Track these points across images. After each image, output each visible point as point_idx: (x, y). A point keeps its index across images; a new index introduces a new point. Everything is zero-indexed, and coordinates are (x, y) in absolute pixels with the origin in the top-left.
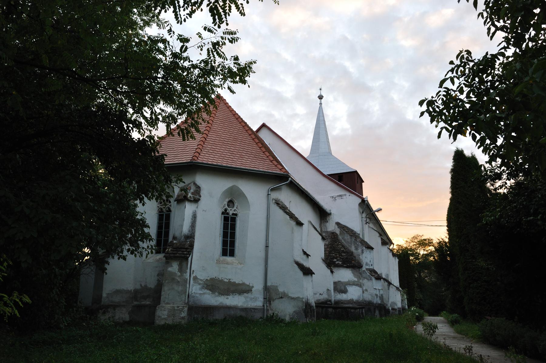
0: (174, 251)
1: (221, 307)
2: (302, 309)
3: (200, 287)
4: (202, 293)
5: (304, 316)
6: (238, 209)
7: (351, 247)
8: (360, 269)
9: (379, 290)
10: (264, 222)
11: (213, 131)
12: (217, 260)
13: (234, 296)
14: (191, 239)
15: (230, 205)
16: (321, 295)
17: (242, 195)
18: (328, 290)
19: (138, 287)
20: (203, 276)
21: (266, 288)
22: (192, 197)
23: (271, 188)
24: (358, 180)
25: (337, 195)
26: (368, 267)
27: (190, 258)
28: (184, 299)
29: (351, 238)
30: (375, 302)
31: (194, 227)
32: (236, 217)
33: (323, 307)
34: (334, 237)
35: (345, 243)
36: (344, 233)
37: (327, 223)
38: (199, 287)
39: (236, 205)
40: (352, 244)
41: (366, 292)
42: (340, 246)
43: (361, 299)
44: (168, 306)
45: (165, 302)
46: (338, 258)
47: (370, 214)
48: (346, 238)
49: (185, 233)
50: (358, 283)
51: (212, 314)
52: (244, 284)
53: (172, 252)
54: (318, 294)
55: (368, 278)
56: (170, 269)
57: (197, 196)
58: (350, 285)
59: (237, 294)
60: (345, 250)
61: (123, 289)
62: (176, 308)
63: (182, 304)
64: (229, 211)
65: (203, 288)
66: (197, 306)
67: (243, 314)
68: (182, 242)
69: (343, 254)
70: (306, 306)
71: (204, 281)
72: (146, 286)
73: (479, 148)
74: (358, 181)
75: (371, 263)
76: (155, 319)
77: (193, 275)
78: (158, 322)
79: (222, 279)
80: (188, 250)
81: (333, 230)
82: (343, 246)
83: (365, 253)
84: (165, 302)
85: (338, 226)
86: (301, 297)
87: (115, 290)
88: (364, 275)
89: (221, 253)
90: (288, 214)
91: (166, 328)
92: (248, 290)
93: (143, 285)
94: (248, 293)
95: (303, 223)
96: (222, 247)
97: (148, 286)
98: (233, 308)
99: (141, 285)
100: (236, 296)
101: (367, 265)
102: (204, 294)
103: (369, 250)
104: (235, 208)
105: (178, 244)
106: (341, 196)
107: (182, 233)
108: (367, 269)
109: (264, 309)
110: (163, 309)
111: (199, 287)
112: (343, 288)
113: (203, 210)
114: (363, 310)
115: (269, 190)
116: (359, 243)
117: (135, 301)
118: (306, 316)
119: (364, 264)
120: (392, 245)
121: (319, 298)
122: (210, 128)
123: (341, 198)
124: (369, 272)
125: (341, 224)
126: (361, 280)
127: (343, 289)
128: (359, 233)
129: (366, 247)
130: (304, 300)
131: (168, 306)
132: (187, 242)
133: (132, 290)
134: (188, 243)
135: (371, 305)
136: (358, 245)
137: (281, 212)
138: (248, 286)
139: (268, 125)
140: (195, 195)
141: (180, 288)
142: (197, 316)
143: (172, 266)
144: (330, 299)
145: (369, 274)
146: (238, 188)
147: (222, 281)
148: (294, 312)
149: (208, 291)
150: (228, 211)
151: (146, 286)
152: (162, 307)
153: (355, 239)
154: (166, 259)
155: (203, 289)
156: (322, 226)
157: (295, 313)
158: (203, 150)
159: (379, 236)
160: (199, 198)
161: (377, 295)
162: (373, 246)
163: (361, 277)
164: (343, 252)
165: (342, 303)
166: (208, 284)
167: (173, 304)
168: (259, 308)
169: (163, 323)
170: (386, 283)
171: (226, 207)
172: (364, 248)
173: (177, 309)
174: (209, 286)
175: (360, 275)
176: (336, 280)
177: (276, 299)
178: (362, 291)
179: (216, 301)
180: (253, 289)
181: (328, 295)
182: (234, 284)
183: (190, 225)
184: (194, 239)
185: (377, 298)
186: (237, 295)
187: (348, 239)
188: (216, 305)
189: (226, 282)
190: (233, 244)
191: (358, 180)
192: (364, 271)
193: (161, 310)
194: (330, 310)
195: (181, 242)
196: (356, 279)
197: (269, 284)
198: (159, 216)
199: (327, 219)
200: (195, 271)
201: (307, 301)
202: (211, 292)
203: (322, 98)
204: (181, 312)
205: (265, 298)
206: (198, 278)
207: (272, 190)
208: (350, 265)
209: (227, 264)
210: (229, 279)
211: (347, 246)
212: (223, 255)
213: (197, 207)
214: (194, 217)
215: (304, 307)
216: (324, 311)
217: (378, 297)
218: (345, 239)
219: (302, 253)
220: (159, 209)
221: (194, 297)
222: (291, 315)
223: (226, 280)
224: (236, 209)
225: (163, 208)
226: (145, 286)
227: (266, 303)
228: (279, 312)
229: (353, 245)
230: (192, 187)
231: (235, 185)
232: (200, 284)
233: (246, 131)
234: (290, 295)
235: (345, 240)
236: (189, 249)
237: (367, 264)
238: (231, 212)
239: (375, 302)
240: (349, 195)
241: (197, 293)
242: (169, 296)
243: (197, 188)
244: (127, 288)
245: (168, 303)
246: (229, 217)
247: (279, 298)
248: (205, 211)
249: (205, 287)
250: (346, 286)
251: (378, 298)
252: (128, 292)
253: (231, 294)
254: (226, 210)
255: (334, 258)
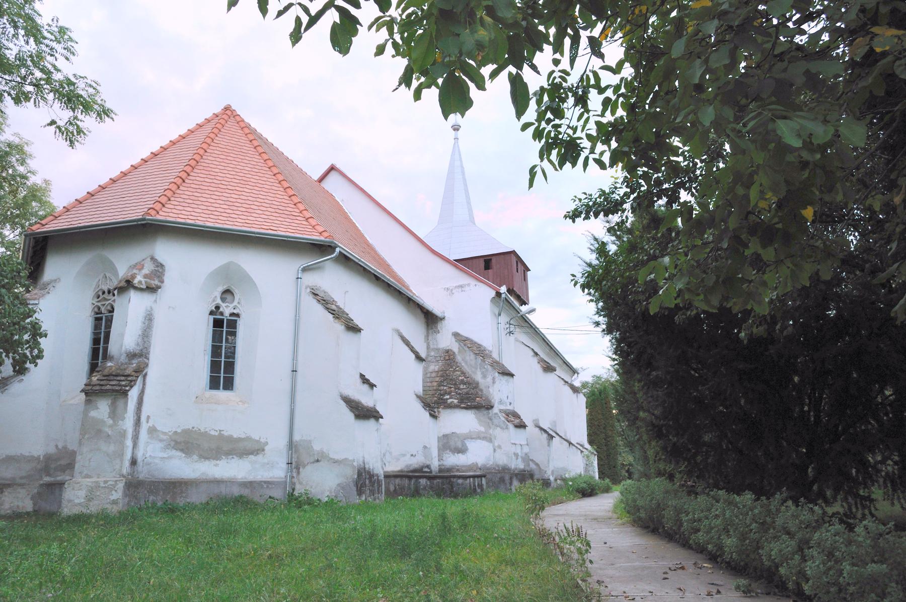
0: (103, 380)
1: (202, 482)
2: (351, 480)
3: (163, 446)
4: (166, 456)
5: (356, 493)
6: (239, 305)
7: (475, 373)
8: (490, 411)
9: (521, 445)
10: (291, 327)
11: (202, 168)
12: (197, 397)
13: (229, 461)
14: (141, 359)
15: (226, 298)
16: (412, 457)
17: (246, 279)
18: (425, 447)
19: (52, 450)
20: (168, 426)
21: (292, 445)
22: (143, 282)
23: (302, 267)
24: (517, 266)
25: (455, 285)
26: (503, 407)
27: (134, 393)
28: (117, 467)
29: (476, 358)
30: (513, 467)
31: (147, 337)
32: (236, 320)
33: (410, 478)
34: (449, 357)
35: (466, 367)
36: (465, 351)
37: (438, 335)
38: (160, 445)
39: (237, 297)
40: (476, 369)
41: (498, 451)
42: (457, 372)
43: (491, 463)
44: (88, 482)
45: (83, 475)
46: (453, 394)
47: (517, 318)
48: (468, 358)
49: (127, 347)
50: (486, 435)
51: (184, 495)
52: (248, 439)
53: (99, 382)
54: (409, 456)
55: (503, 425)
56: (93, 414)
57: (154, 280)
58: (472, 439)
59: (234, 456)
60: (465, 379)
61: (21, 454)
62: (102, 485)
63: (115, 477)
64: (224, 309)
65: (167, 447)
66: (157, 480)
67: (246, 492)
68: (122, 364)
69: (462, 387)
70: (360, 474)
71: (170, 436)
72: (65, 448)
73: (688, 194)
74: (517, 269)
75: (509, 400)
76: (62, 505)
77: (149, 425)
78: (67, 510)
79: (207, 430)
80: (130, 378)
81: (448, 346)
82: (463, 373)
83: (497, 382)
84: (83, 475)
85: (455, 338)
86: (351, 458)
87: (4, 456)
88: (496, 421)
89: (207, 384)
90: (332, 312)
91: (80, 520)
92: (258, 450)
93: (60, 447)
94: (258, 454)
95: (362, 328)
96: (209, 374)
97: (68, 447)
98: (226, 481)
99: (57, 446)
100: (233, 460)
101: (501, 404)
102: (170, 458)
103: (506, 378)
104: (235, 303)
105: (114, 368)
106: (461, 286)
107: (122, 348)
108: (501, 411)
109: (286, 482)
110: (77, 486)
111: (161, 445)
112: (459, 445)
113: (170, 307)
114: (481, 480)
115: (298, 270)
116: (489, 366)
117: (46, 476)
118: (360, 492)
119: (497, 402)
120: (576, 374)
121: (410, 463)
122: (198, 162)
123: (462, 291)
124: (504, 415)
125: (462, 336)
126: (491, 430)
127: (460, 446)
128: (490, 349)
129: (499, 373)
130: (355, 464)
131: (88, 482)
132: (132, 364)
133: (42, 457)
134: (135, 365)
135: (506, 471)
136: (487, 370)
137: (319, 309)
138: (258, 442)
139: (338, 166)
140: (150, 279)
141: (112, 448)
142: (155, 498)
143: (98, 408)
144: (428, 463)
145: (503, 419)
146: (239, 266)
147: (205, 435)
148: (339, 485)
149: (179, 453)
150: (221, 310)
151: (65, 448)
152: (75, 483)
153: (482, 360)
154: (87, 394)
155: (167, 450)
156: (430, 339)
157: (339, 488)
158: (172, 199)
159: (534, 356)
160: (159, 284)
161: (516, 455)
162: (514, 373)
163: (490, 424)
164: (462, 382)
165: (458, 470)
166: (179, 441)
167: (98, 478)
168: (277, 482)
169: (76, 510)
170: (545, 436)
171: (219, 301)
172: (497, 374)
173: (104, 486)
174: (180, 443)
175: (490, 422)
176: (447, 431)
177: (308, 463)
178: (493, 449)
179: (193, 471)
180: (267, 448)
181: (425, 457)
182: (230, 439)
183: (140, 333)
184: (148, 359)
185: (517, 459)
186: (236, 458)
187: (471, 360)
188: (194, 477)
189: (215, 435)
190: (230, 367)
191: (517, 266)
192: (496, 414)
193: (73, 489)
194: (423, 481)
195: (120, 364)
196: (483, 429)
197: (297, 437)
198: (95, 320)
199: (439, 327)
200: (151, 417)
201: (362, 464)
202: (184, 455)
203: (458, 130)
204: (111, 491)
205: (288, 464)
206: (158, 429)
207: (305, 270)
208: (473, 404)
209: (216, 403)
210: (220, 431)
211: (470, 373)
212: (211, 388)
213: (156, 301)
214: (149, 319)
215: (356, 477)
216: (412, 483)
217: (519, 457)
218: (467, 361)
219: (359, 380)
220: (94, 308)
221: (149, 464)
222: (333, 491)
223: (213, 433)
224: (238, 305)
225: (101, 306)
226: (63, 447)
227: (291, 471)
228: (313, 487)
229: (479, 370)
230: (146, 265)
231: (231, 262)
232: (161, 441)
233: (269, 168)
234: (331, 456)
235: (466, 363)
236: (132, 376)
237: (501, 402)
238: (227, 310)
239: (513, 467)
240: (476, 285)
241: (154, 457)
242: (90, 462)
243: (157, 266)
244: (30, 452)
245: (87, 476)
246: (224, 319)
247: (313, 463)
248: (173, 308)
249: (172, 445)
250: (466, 441)
251: (520, 460)
252: (31, 459)
253: (224, 457)
254: (217, 308)
255: (446, 393)
